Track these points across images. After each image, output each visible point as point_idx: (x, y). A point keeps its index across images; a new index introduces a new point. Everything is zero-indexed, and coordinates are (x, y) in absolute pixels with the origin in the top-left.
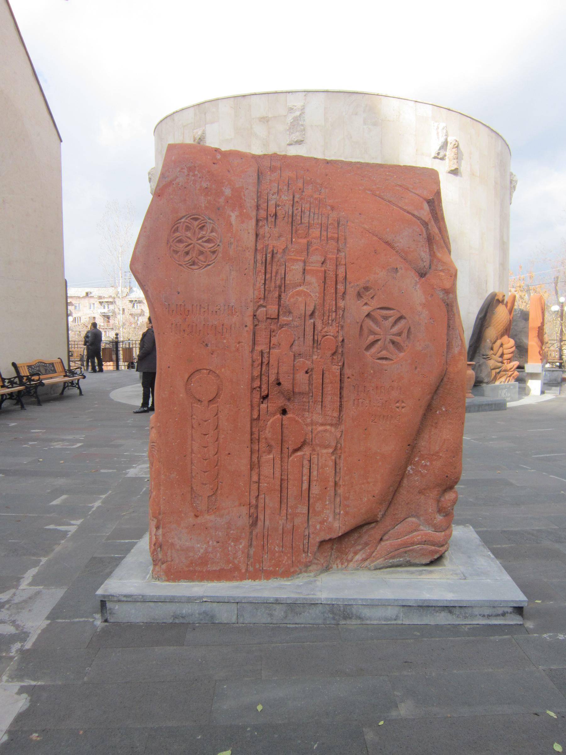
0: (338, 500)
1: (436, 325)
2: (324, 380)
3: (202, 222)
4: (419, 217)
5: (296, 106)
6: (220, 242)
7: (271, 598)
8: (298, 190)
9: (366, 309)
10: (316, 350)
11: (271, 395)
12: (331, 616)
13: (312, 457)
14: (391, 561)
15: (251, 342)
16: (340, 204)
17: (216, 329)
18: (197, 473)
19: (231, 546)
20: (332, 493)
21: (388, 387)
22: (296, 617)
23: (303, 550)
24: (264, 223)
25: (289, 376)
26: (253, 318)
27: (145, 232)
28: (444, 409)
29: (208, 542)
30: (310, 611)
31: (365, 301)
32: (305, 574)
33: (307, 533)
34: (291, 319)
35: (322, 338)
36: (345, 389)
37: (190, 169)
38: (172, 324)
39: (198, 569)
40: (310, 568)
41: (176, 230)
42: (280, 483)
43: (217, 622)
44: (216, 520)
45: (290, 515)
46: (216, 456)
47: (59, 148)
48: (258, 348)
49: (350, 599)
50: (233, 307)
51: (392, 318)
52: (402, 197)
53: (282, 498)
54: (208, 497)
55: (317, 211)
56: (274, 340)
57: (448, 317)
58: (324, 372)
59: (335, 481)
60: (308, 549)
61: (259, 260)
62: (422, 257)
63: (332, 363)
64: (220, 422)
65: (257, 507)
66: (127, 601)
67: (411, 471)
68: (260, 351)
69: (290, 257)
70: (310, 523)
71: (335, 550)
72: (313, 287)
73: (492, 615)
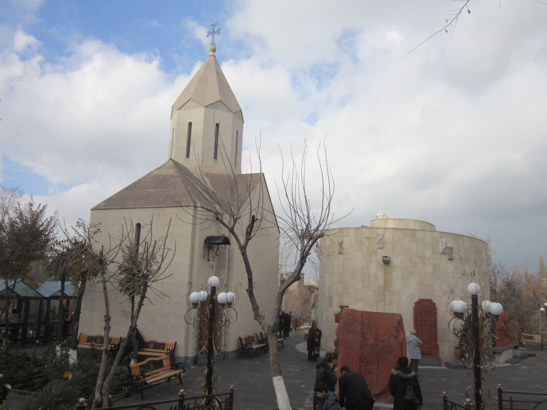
9: (383, 345)
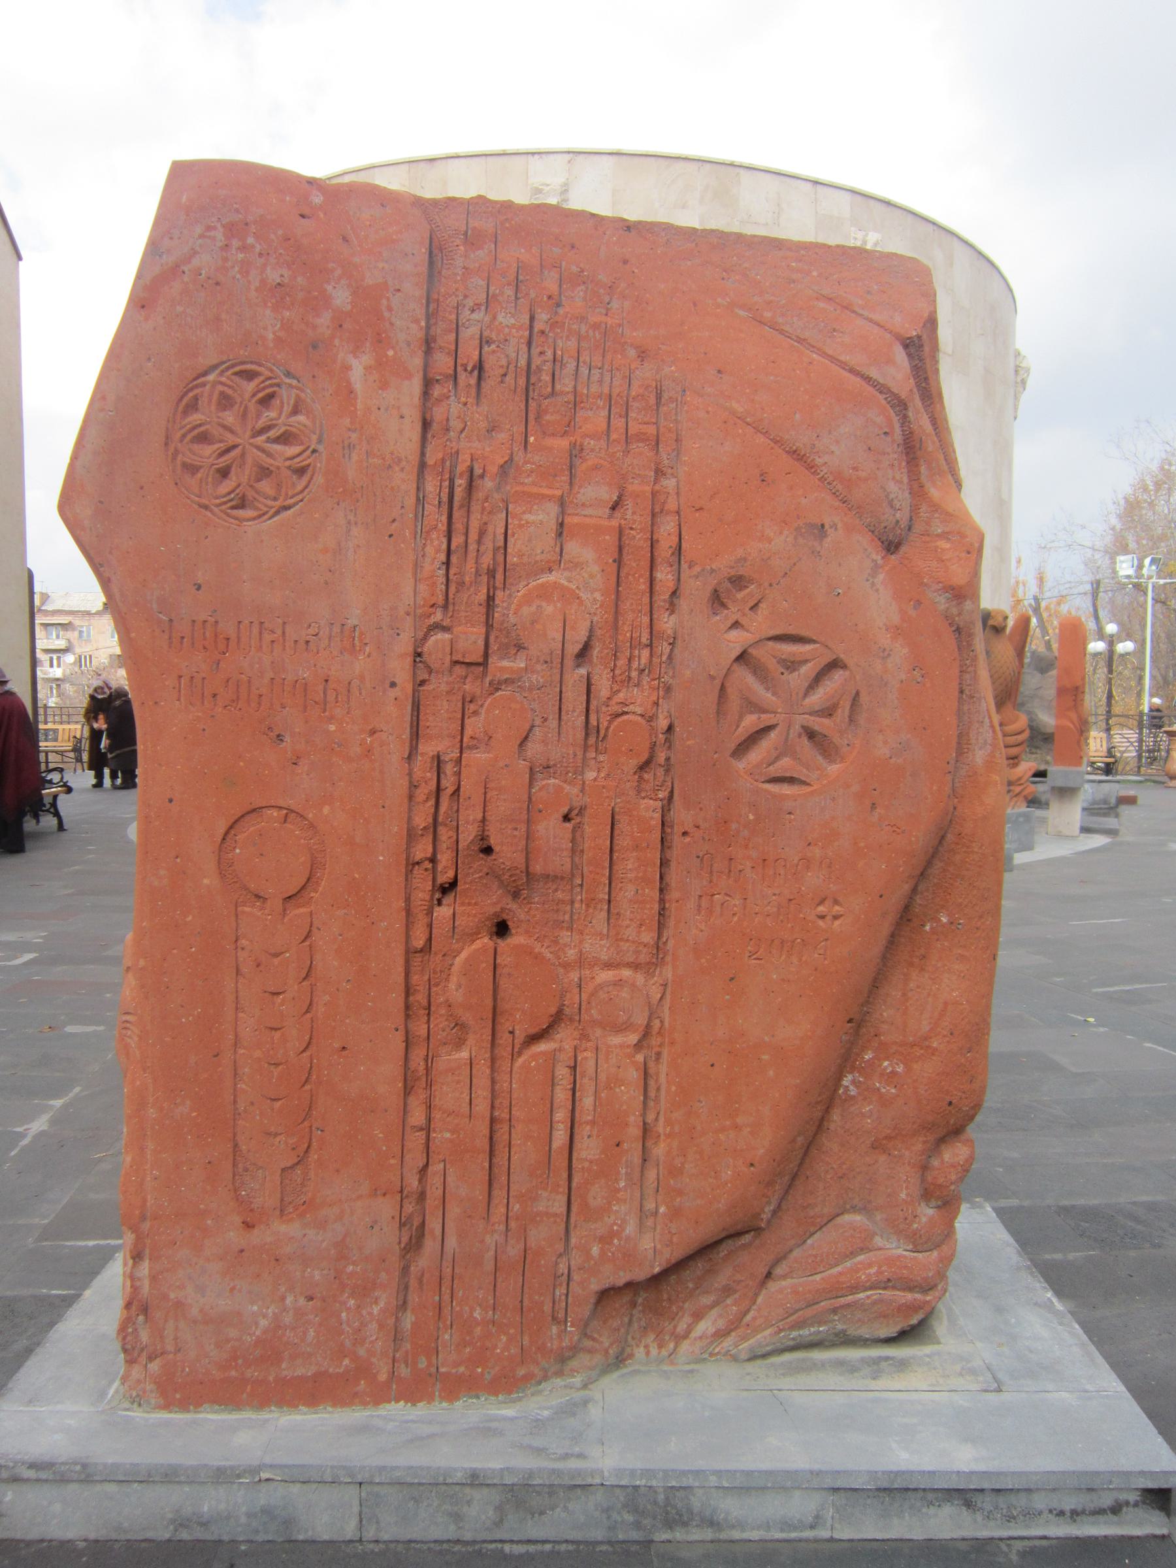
0: (651, 1175)
1: (928, 685)
2: (615, 842)
3: (267, 383)
4: (882, 385)
5: (548, 185)
6: (320, 441)
7: (455, 1470)
8: (545, 299)
9: (737, 640)
10: (593, 755)
11: (465, 883)
12: (630, 1518)
13: (579, 1058)
14: (794, 1334)
15: (408, 730)
16: (663, 344)
17: (305, 690)
18: (252, 1104)
19: (348, 1309)
20: (637, 1160)
21: (795, 862)
22: (530, 1523)
23: (553, 1316)
24: (445, 391)
25: (516, 829)
26: (415, 661)
27: (102, 410)
28: (944, 920)
29: (283, 1299)
30: (570, 1506)
31: (734, 618)
32: (558, 1380)
33: (563, 1268)
34: (523, 665)
35: (610, 722)
36: (673, 864)
37: (231, 230)
38: (180, 677)
39: (252, 1373)
40: (574, 1363)
41: (193, 406)
42: (488, 1130)
43: (301, 1537)
44: (305, 1235)
45: (517, 1219)
46: (305, 1054)
47: (16, 269)
48: (428, 748)
49: (684, 1473)
50: (354, 631)
51: (809, 665)
52: (834, 330)
53: (496, 1170)
54: (283, 1170)
55: (597, 360)
56: (475, 725)
57: (961, 666)
58: (617, 817)
59: (645, 1123)
60: (566, 1310)
61: (431, 496)
62: (892, 496)
63: (639, 792)
64: (318, 957)
65: (422, 1196)
66: (38, 1480)
67: (851, 1087)
68: (433, 757)
69: (518, 488)
70: (573, 1241)
71: (640, 1308)
72: (586, 576)
73: (1083, 1512)
